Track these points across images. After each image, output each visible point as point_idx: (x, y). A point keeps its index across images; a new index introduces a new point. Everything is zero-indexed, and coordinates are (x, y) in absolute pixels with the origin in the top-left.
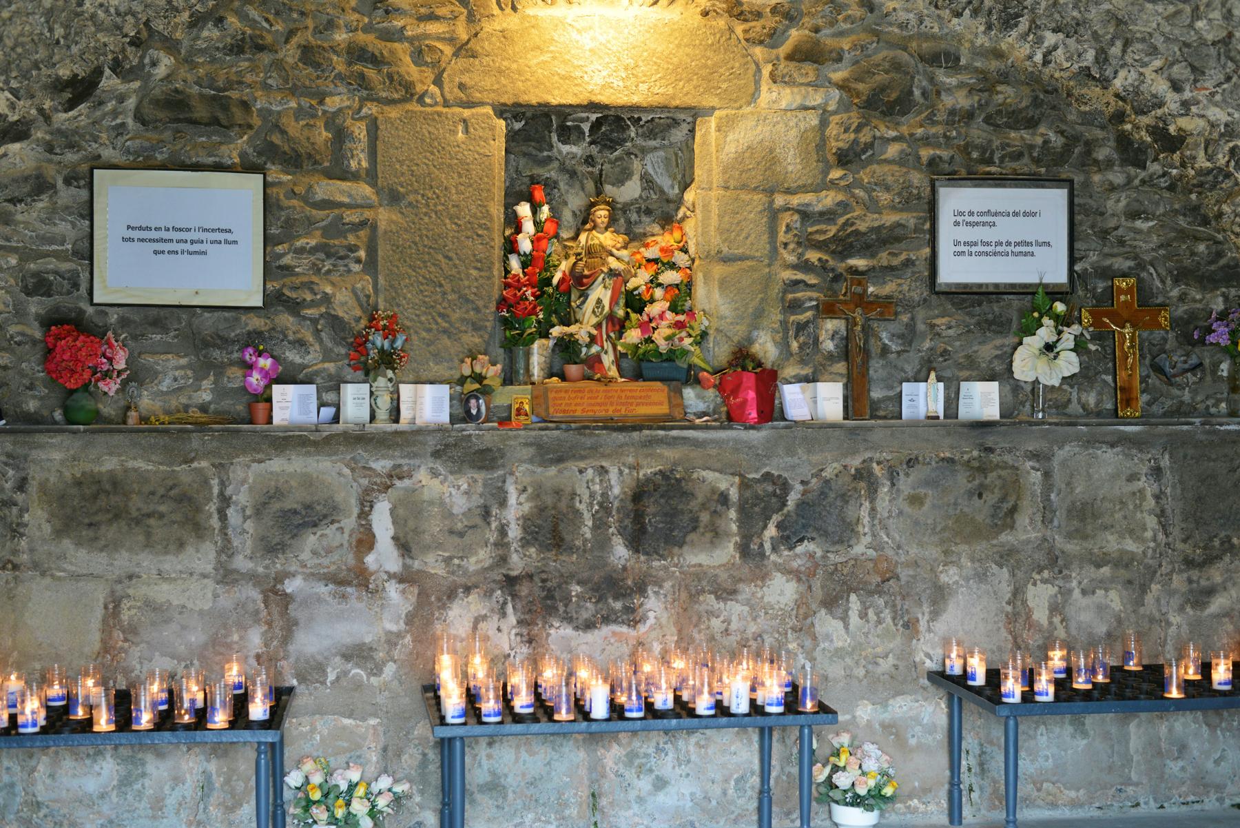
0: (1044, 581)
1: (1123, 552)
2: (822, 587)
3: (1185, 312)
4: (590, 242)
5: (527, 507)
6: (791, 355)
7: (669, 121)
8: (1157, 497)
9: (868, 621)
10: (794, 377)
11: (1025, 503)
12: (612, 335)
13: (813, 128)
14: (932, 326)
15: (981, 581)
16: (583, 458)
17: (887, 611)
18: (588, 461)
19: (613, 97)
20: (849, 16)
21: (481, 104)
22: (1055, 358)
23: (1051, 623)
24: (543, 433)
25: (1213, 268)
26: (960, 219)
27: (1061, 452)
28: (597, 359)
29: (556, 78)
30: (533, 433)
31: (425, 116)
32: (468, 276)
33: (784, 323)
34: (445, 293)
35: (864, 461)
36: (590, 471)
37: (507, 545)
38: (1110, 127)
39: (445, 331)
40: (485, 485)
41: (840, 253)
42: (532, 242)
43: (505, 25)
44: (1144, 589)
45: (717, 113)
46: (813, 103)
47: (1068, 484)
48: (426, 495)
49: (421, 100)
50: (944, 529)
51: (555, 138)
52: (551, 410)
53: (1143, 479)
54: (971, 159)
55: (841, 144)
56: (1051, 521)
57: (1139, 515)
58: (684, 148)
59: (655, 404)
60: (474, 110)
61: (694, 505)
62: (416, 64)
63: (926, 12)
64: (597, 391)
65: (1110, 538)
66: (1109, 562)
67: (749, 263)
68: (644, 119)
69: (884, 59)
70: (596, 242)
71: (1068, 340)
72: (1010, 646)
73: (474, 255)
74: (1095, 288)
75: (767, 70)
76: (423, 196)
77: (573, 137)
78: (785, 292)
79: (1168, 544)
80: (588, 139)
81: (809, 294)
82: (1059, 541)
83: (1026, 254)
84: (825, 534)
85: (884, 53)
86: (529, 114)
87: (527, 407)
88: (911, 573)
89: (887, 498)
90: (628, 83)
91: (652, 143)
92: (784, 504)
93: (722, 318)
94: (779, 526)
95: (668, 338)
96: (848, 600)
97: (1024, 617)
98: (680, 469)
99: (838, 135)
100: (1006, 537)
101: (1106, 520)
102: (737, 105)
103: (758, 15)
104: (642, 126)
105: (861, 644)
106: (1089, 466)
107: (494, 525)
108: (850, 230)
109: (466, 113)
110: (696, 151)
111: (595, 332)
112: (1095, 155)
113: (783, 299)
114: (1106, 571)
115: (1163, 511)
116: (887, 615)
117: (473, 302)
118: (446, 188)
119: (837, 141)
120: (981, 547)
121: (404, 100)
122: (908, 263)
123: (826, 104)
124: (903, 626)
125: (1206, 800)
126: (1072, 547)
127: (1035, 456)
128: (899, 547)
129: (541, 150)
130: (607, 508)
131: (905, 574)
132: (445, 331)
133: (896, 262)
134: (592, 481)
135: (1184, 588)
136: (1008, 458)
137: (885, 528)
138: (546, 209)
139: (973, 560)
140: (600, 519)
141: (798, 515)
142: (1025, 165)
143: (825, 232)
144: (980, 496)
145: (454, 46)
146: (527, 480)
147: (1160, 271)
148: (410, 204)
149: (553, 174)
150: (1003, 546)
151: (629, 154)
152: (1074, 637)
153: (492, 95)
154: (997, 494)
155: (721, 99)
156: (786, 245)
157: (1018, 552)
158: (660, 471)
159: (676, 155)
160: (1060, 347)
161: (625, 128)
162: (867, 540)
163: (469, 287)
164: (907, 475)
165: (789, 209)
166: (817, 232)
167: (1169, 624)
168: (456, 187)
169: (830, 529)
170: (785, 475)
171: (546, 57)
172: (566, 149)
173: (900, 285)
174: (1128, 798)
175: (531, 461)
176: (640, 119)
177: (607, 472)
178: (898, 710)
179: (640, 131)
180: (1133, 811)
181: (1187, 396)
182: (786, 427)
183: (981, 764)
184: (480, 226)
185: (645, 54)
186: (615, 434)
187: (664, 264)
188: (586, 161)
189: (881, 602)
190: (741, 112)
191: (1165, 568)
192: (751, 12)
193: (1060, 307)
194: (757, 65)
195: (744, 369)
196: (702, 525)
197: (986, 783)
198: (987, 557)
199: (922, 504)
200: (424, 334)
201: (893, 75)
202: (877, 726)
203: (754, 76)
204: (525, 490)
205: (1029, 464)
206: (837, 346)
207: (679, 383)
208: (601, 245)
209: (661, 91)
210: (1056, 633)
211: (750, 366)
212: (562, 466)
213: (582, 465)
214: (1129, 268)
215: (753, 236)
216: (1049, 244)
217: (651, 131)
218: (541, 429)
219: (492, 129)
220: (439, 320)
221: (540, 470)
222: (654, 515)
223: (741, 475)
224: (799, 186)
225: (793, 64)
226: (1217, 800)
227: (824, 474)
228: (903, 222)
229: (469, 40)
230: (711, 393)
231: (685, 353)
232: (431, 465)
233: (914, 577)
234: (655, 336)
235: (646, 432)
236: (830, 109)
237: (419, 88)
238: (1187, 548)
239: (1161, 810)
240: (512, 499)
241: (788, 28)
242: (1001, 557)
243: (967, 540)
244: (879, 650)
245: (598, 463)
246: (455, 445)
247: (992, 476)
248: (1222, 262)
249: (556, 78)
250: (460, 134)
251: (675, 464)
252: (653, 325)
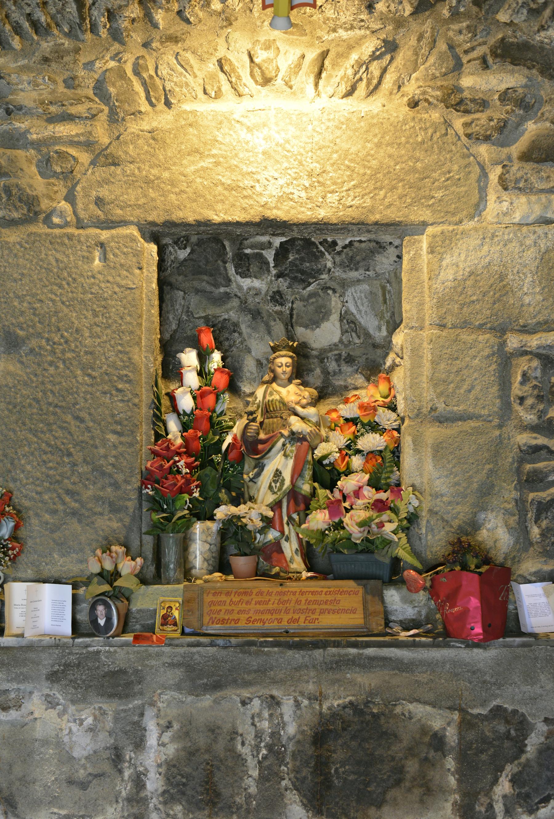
4: (268, 398)
5: (171, 750)
6: (531, 544)
7: (373, 244)
10: (535, 573)
12: (295, 516)
16: (247, 684)
18: (253, 689)
19: (293, 212)
21: (123, 223)
24: (194, 650)
28: (277, 547)
29: (220, 188)
30: (181, 650)
31: (52, 241)
32: (104, 441)
33: (520, 503)
34: (75, 465)
36: (256, 702)
37: (144, 801)
39: (74, 513)
40: (116, 720)
42: (194, 398)
43: (155, 124)
45: (430, 230)
48: (39, 732)
49: (47, 220)
51: (231, 270)
52: (206, 619)
58: (393, 280)
59: (345, 611)
60: (114, 232)
61: (397, 750)
62: (42, 174)
64: (269, 593)
67: (472, 424)
68: (341, 243)
70: (276, 397)
73: (113, 416)
75: (494, 174)
76: (48, 340)
77: (254, 268)
78: (521, 461)
80: (274, 272)
86: (194, 239)
87: (176, 614)
90: (313, 194)
91: (354, 275)
92: (522, 750)
93: (436, 496)
94: (514, 780)
95: (362, 524)
98: (378, 700)
102: (456, 219)
103: (484, 104)
104: (339, 253)
107: (127, 774)
109: (105, 235)
110: (404, 280)
111: (270, 514)
113: (519, 471)
117: (110, 476)
118: (77, 331)
121: (25, 221)
129: (216, 285)
130: (279, 753)
132: (74, 513)
134: (259, 715)
138: (217, 356)
140: (269, 768)
141: (540, 765)
145: (93, 152)
146: (172, 712)
148: (32, 350)
149: (233, 315)
151: (325, 288)
153: (138, 212)
155: (434, 212)
156: (522, 399)
158: (351, 703)
159: (383, 288)
161: (318, 256)
163: (106, 457)
165: (526, 353)
168: (90, 329)
170: (523, 710)
171: (207, 163)
172: (246, 283)
175: (178, 687)
176: (335, 243)
177: (278, 704)
179: (338, 259)
182: (524, 645)
184: (120, 378)
185: (335, 156)
186: (290, 653)
187: (363, 425)
188: (273, 299)
190: (461, 228)
192: (473, 100)
194: (482, 168)
195: (465, 567)
196: (408, 776)
200: (47, 517)
203: (479, 181)
204: (169, 726)
207: (379, 583)
208: (282, 402)
209: (356, 202)
211: (472, 563)
212: (219, 694)
213: (246, 693)
215: (478, 388)
217: (351, 259)
218: (190, 645)
219: (138, 254)
220: (67, 499)
221: (190, 698)
222: (343, 765)
223: (462, 710)
224: (539, 323)
225: (529, 166)
229: (110, 144)
230: (422, 596)
231: (388, 543)
232: (47, 691)
234: (347, 520)
235: (334, 650)
237: (45, 204)
240: (152, 740)
241: (523, 120)
245: (267, 692)
246: (78, 665)
249: (220, 188)
250: (97, 262)
251: (371, 694)
252: (347, 505)
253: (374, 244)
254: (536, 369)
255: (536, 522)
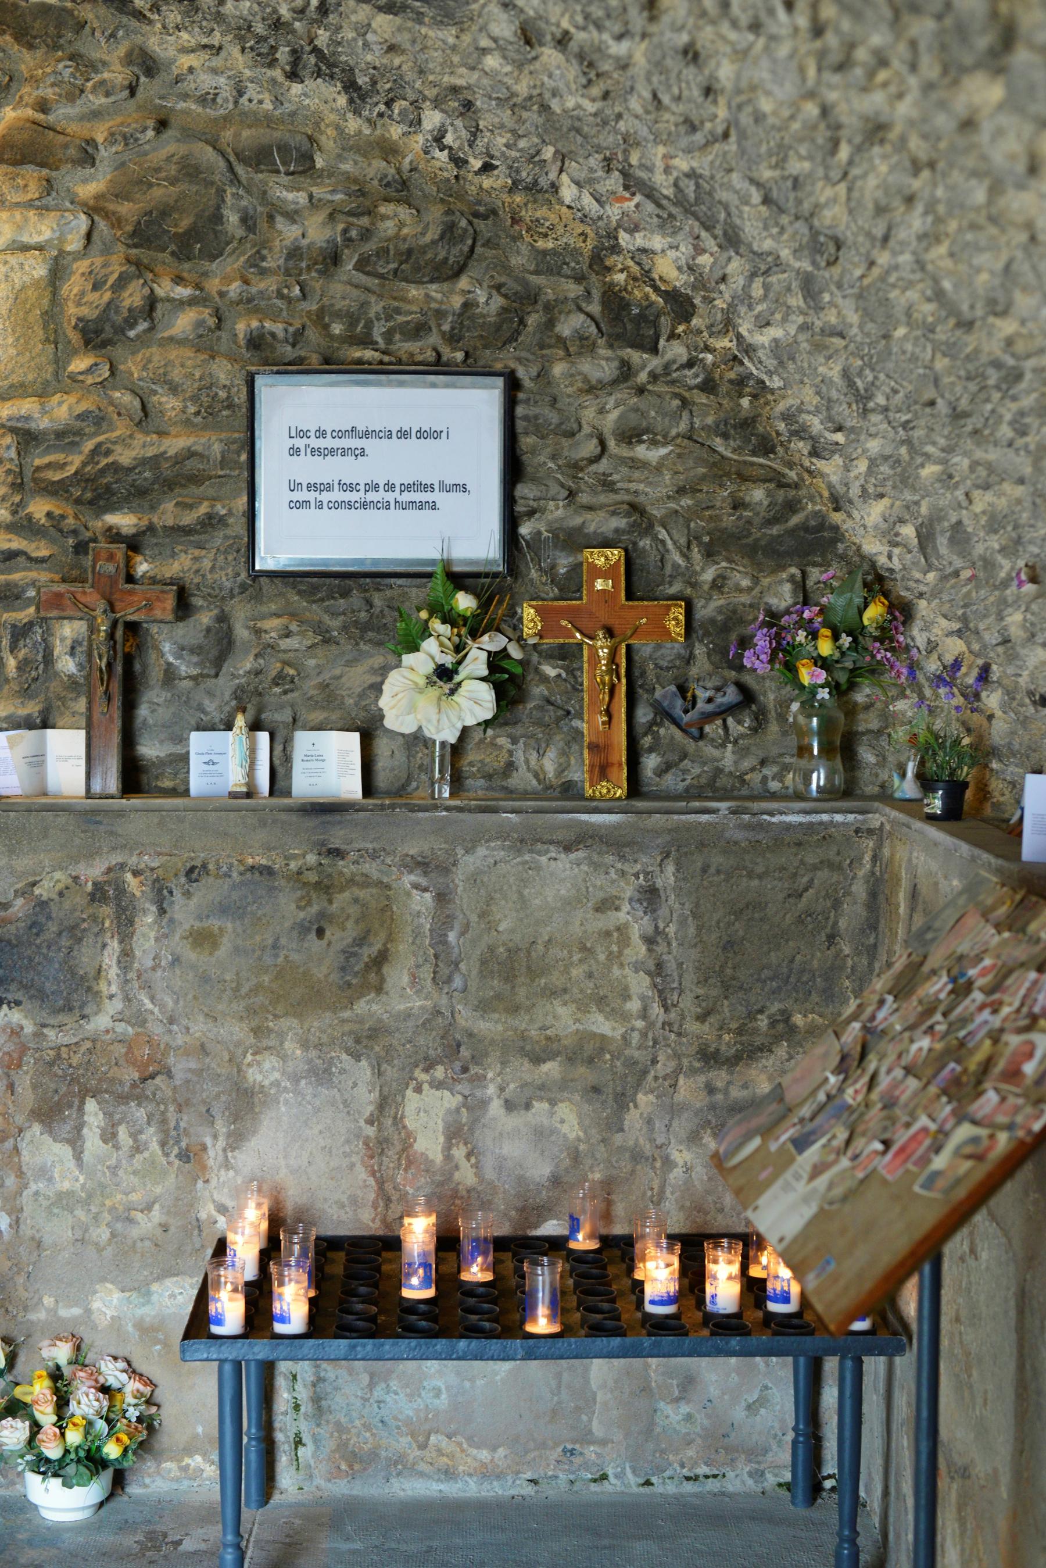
0: (438, 1085)
1: (585, 1037)
2: (35, 1087)
3: (720, 610)
8: (650, 941)
9: (117, 1147)
11: (402, 948)
13: (36, 283)
14: (258, 632)
15: (320, 1082)
17: (152, 1130)
20: (102, 82)
22: (453, 692)
23: (448, 1157)
25: (775, 530)
26: (300, 443)
27: (469, 859)
35: (109, 870)
38: (594, 278)
41: (91, 503)
44: (623, 1101)
46: (36, 239)
47: (483, 915)
50: (256, 990)
53: (626, 907)
54: (332, 337)
55: (85, 311)
56: (449, 980)
57: (616, 972)
63: (248, 73)
65: (561, 1011)
66: (558, 1054)
69: (169, 159)
71: (476, 662)
72: (372, 1196)
74: (553, 567)
79: (667, 1025)
81: (33, 575)
82: (466, 1017)
83: (421, 506)
84: (40, 996)
85: (171, 148)
88: (193, 1065)
89: (152, 934)
96: (81, 1109)
97: (398, 1147)
99: (82, 293)
100: (367, 1007)
101: (556, 979)
105: (103, 1186)
106: (524, 882)
108: (104, 462)
112: (558, 328)
114: (551, 1068)
115: (659, 966)
116: (151, 1136)
119: (79, 304)
120: (320, 1023)
122: (211, 522)
123: (62, 239)
124: (179, 1156)
125: (731, 1475)
126: (488, 1026)
127: (421, 864)
128: (172, 1021)
131: (181, 1067)
133: (188, 519)
135: (700, 1101)
136: (371, 868)
137: (148, 986)
139: (305, 1045)
142: (421, 349)
143: (62, 466)
144: (320, 933)
147: (676, 537)
150: (361, 1021)
152: (491, 1183)
154: (351, 931)
157: (389, 1032)
160: (463, 672)
162: (116, 1005)
164: (187, 894)
166: (49, 466)
167: (668, 1163)
169: (49, 987)
173: (196, 559)
174: (586, 1466)
178: (167, 1301)
180: (594, 1487)
181: (728, 758)
183: (317, 1400)
189: (140, 1114)
191: (664, 1065)
193: (464, 602)
197: (323, 1431)
198: (332, 1042)
199: (215, 945)
201: (182, 186)
202: (130, 1328)
205: (408, 879)
206: (80, 666)
210: (457, 1176)
214: (617, 531)
216: (464, 488)
224: (11, 386)
226: (750, 1474)
227: (37, 891)
228: (199, 448)
233: (198, 1073)
236: (69, 248)
238: (705, 1031)
239: (647, 1490)
242: (358, 1041)
243: (299, 1009)
244: (134, 1197)
247: (342, 899)
248: (795, 520)
253: (137, 403)
254: (8, 447)
255: (12, 652)
